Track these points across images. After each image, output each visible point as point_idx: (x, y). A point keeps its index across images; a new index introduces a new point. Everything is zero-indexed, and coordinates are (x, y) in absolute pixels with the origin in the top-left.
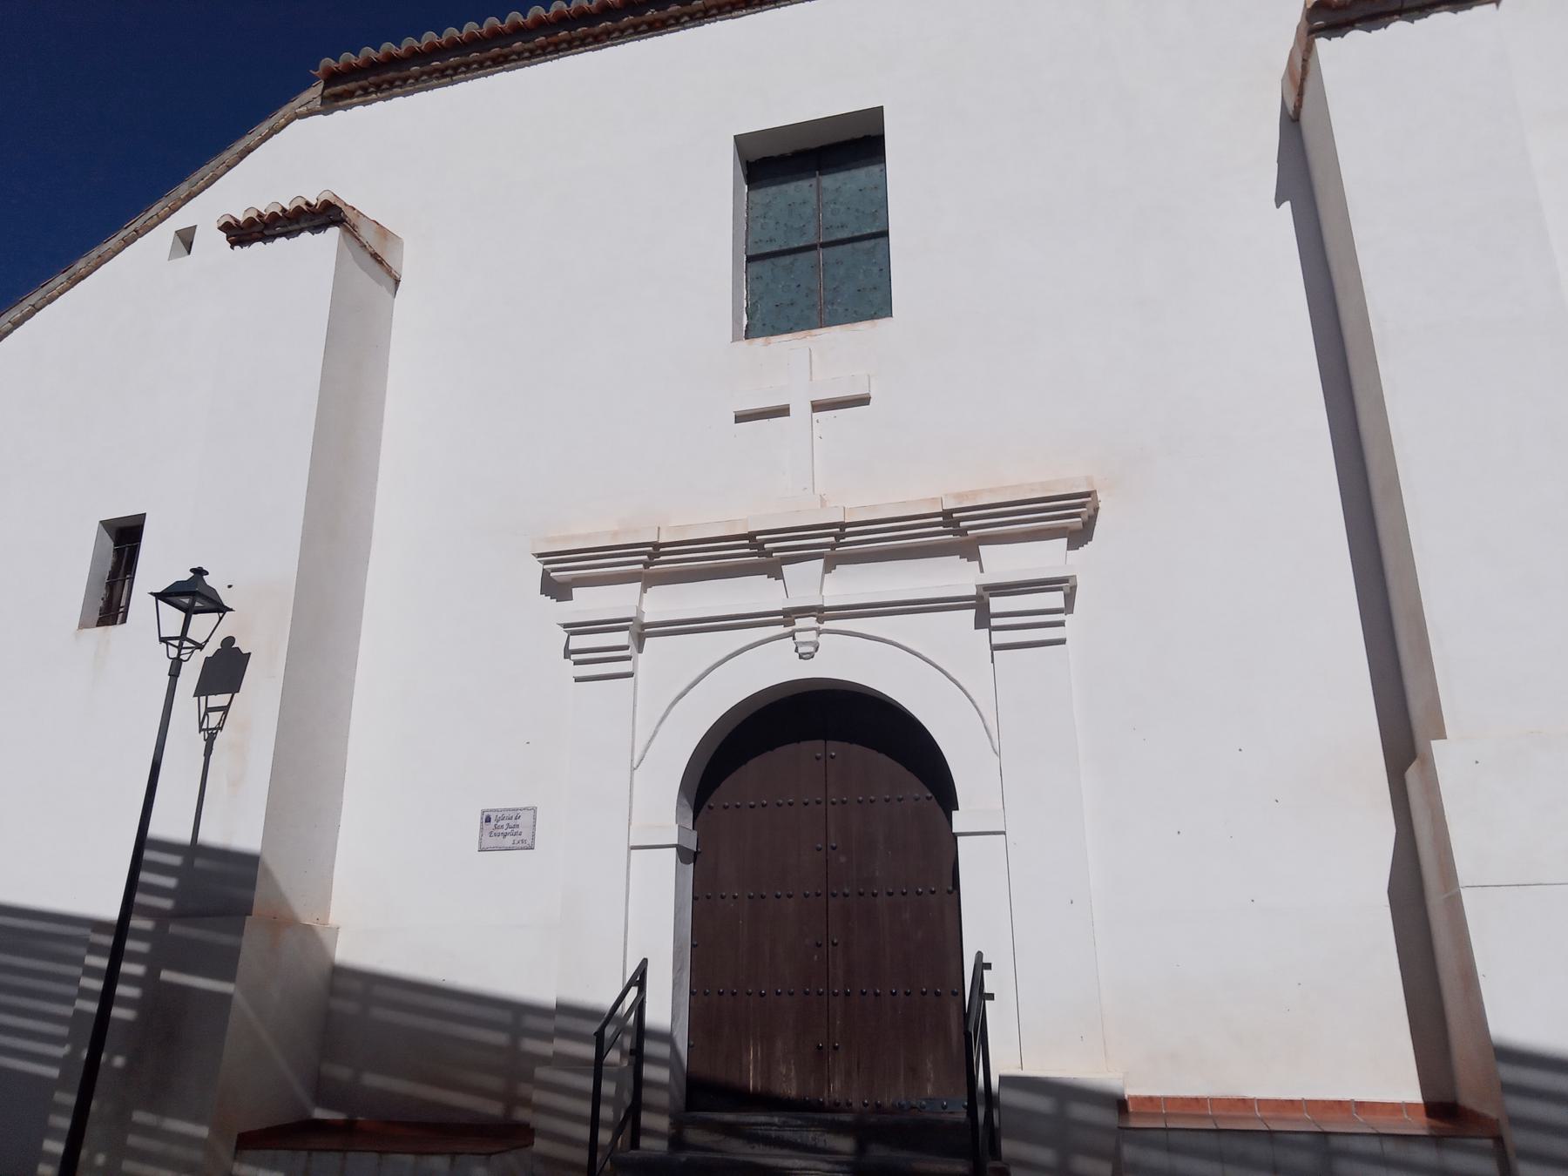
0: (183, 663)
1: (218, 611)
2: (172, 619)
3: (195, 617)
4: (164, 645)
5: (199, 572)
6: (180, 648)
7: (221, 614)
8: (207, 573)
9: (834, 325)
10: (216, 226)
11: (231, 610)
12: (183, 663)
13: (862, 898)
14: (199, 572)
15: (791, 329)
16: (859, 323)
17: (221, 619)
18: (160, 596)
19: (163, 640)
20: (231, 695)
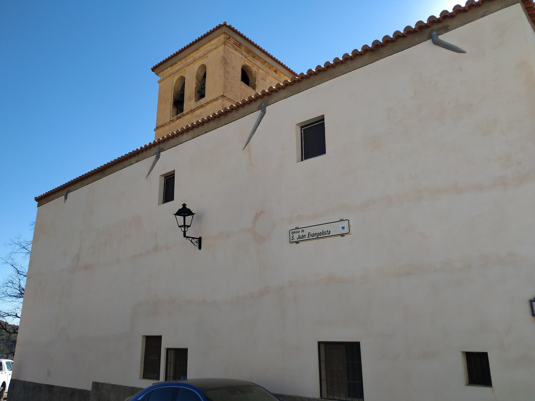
0: (186, 232)
1: (191, 215)
2: (180, 218)
3: (186, 217)
4: (180, 228)
5: (184, 205)
6: (185, 227)
7: (192, 215)
8: (186, 205)
9: (441, 47)
10: (200, 250)
11: (195, 214)
12: (186, 232)
13: (343, 226)
14: (184, 205)
15: (461, 25)
16: (441, 47)
17: (193, 217)
18: (176, 215)
19: (179, 227)
20: (258, 113)
